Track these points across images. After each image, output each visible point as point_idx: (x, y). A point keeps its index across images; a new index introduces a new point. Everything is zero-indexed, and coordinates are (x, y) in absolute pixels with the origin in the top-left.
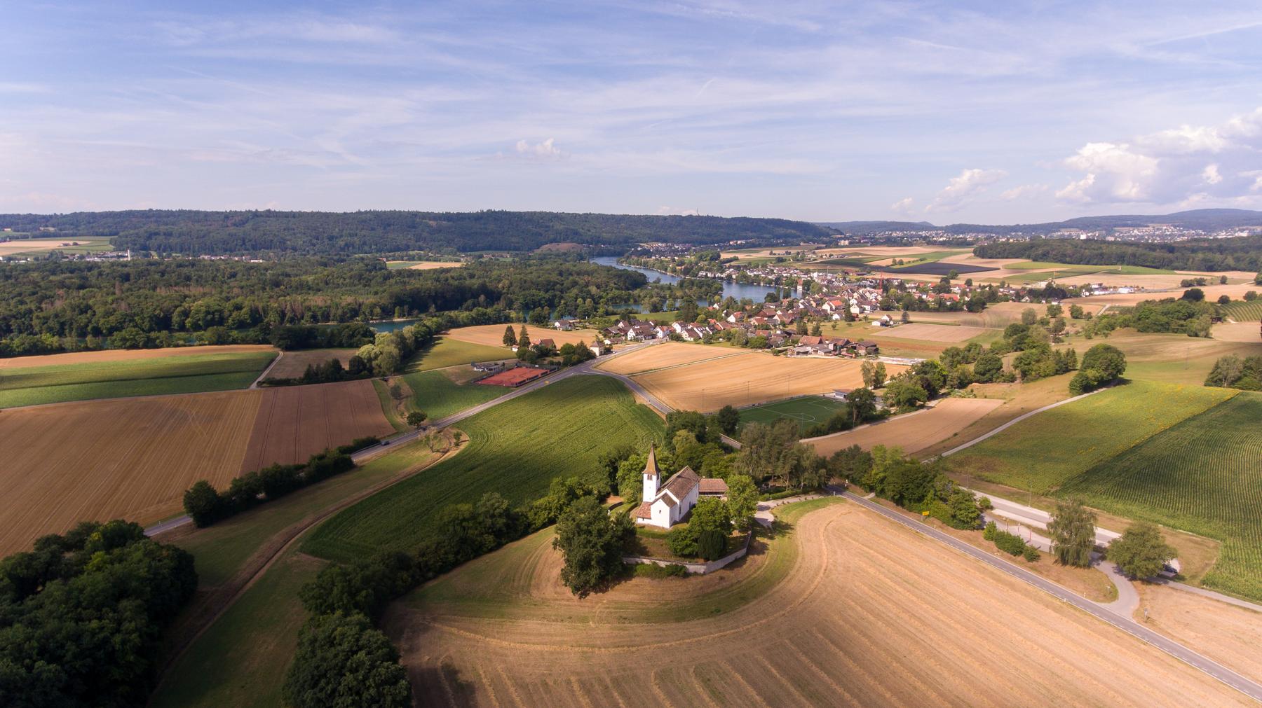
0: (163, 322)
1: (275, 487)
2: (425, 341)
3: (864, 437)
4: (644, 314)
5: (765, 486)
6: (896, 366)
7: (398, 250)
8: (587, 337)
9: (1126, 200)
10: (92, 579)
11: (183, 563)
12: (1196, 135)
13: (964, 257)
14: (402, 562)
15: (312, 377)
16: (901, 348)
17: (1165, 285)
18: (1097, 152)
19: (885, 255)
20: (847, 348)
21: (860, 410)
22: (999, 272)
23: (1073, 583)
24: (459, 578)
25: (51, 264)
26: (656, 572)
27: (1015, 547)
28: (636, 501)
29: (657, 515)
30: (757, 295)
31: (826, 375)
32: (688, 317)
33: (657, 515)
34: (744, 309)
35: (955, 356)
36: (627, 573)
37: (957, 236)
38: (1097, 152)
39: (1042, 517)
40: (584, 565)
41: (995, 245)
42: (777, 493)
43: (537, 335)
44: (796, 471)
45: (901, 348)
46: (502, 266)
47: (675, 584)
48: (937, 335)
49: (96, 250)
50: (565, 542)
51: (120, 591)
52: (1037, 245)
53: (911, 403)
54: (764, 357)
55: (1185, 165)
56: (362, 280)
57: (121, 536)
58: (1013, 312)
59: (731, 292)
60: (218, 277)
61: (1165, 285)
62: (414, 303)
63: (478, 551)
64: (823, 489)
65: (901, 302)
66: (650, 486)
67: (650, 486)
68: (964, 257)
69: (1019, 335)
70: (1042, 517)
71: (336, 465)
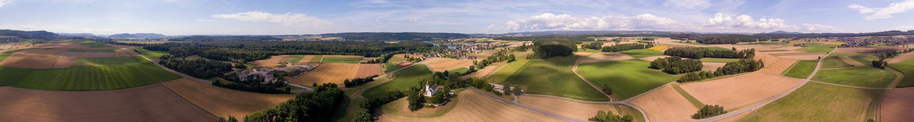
0: (347, 51)
1: (358, 82)
2: (390, 57)
3: (472, 76)
4: (432, 52)
5: (452, 87)
6: (479, 60)
7: (388, 40)
8: (420, 56)
9: (747, 27)
10: (328, 92)
11: (342, 93)
12: (523, 21)
13: (491, 40)
14: (378, 100)
15: (369, 62)
16: (480, 57)
17: (521, 44)
18: (510, 22)
19: (479, 40)
20: (471, 58)
21: (472, 70)
22: (498, 42)
23: (507, 99)
24: (388, 105)
25: (334, 41)
26: (428, 107)
27: (498, 94)
28: (425, 91)
29: (429, 94)
30: (454, 48)
31: (464, 64)
32: (441, 52)
33: (429, 94)
34: (452, 51)
35: (489, 58)
36: (422, 107)
37: (490, 36)
38: (510, 22)
39: (502, 87)
40: (413, 105)
41: (497, 38)
42: (455, 88)
43: (411, 56)
44: (458, 83)
45: (480, 57)
46: (406, 43)
47: (432, 109)
48: (486, 54)
49: (340, 39)
50: (409, 99)
51: (331, 95)
52: (503, 38)
53: (482, 68)
54: (455, 60)
55: (522, 25)
56: (380, 45)
57: (334, 86)
58: (499, 49)
59: (450, 47)
60: (357, 44)
61: (521, 44)
62: (388, 50)
63: (393, 100)
64: (464, 87)
65: (480, 48)
66: (427, 87)
67: (427, 87)
68: (491, 40)
69: (500, 54)
70: (502, 87)
71: (370, 79)
